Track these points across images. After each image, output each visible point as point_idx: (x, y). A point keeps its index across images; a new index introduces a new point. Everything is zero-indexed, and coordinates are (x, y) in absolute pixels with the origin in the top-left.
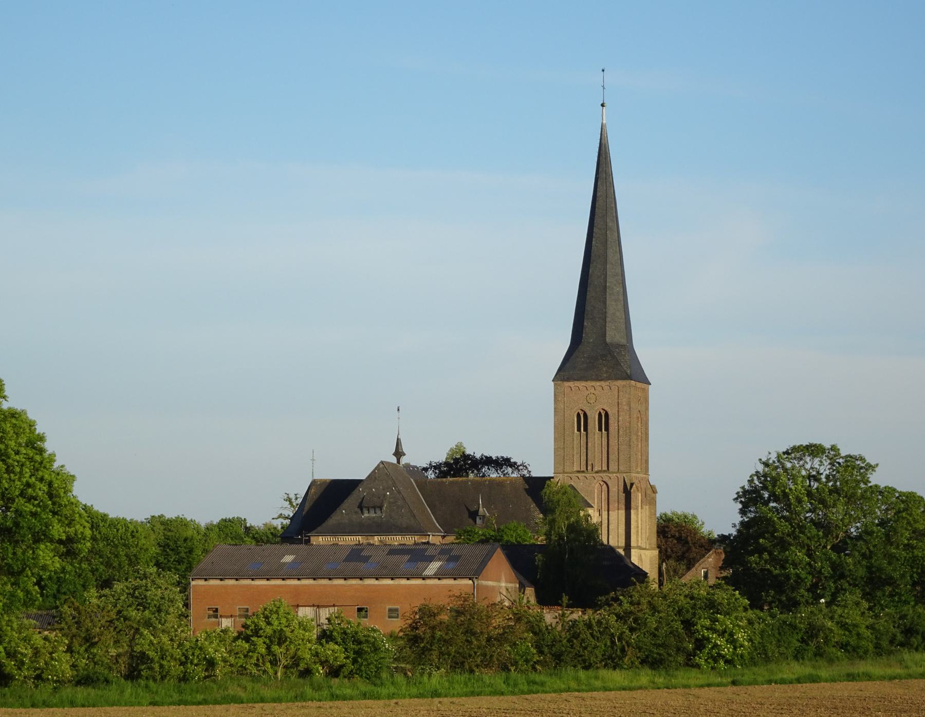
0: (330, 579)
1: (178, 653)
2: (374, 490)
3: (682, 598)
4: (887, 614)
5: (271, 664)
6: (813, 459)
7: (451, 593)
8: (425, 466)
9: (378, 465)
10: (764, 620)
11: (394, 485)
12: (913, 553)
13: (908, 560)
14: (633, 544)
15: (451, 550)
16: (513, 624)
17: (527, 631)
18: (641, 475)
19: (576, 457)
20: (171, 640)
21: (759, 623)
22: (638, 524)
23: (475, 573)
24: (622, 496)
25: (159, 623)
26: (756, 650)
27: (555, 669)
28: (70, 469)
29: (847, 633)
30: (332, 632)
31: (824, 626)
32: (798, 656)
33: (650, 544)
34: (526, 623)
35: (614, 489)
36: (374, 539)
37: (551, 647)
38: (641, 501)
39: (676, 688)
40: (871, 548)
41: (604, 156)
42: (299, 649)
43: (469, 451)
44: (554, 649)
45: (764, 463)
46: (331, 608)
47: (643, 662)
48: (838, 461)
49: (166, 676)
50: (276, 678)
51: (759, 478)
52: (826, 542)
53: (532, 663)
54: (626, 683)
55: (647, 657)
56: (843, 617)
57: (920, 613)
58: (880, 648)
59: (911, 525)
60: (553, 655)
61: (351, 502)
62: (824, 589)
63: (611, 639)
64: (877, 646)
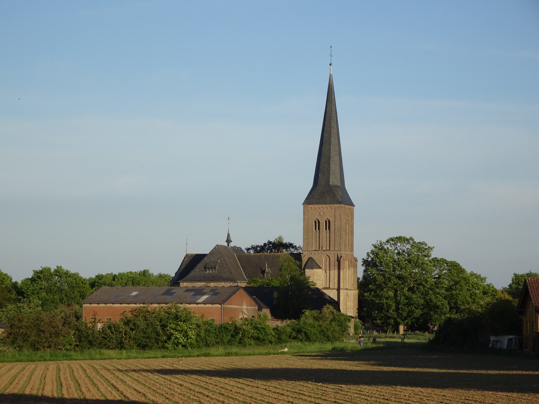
2: (212, 259)
8: (249, 247)
9: (215, 247)
14: (341, 287)
19: (314, 243)
24: (337, 263)
33: (353, 287)
58: (280, 340)
61: (200, 265)
64: (279, 339)
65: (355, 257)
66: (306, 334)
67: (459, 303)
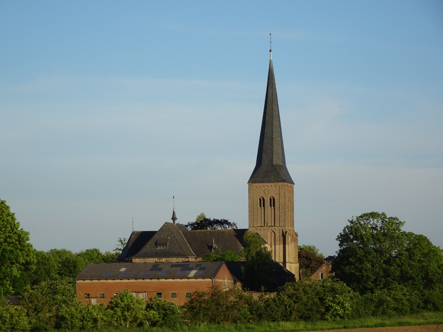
0: (143, 279)
1: (79, 316)
2: (162, 236)
3: (319, 287)
4: (416, 294)
5: (123, 321)
6: (374, 219)
7: (208, 286)
8: (186, 224)
9: (164, 224)
10: (358, 297)
11: (172, 233)
12: (422, 264)
13: (420, 268)
14: (287, 261)
15: (201, 265)
16: (238, 300)
17: (245, 304)
18: (290, 228)
19: (259, 220)
20: (76, 309)
21: (355, 299)
22: (289, 251)
23: (213, 276)
24: (282, 238)
25: (70, 301)
26: (354, 311)
27: (258, 322)
28: (25, 230)
29: (397, 303)
30: (152, 305)
31: (386, 300)
32: (374, 314)
33: (295, 261)
34: (245, 300)
35: (277, 235)
36: (163, 260)
37: (256, 311)
38: (291, 240)
39: (317, 330)
40: (402, 261)
41: (271, 75)
42: (137, 313)
43: (207, 217)
44: (258, 312)
45: (350, 222)
46: (144, 293)
47: (301, 318)
48: (385, 220)
49: (74, 327)
50: (126, 327)
51: (348, 229)
52: (381, 259)
53: (247, 319)
54: (293, 328)
55: (302, 315)
56: (395, 295)
57: (431, 293)
58: (412, 310)
59: (421, 251)
60: (257, 315)
61: (151, 242)
62: (380, 281)
63: (285, 307)
64: (411, 309)
66: (434, 304)
67: (430, 274)
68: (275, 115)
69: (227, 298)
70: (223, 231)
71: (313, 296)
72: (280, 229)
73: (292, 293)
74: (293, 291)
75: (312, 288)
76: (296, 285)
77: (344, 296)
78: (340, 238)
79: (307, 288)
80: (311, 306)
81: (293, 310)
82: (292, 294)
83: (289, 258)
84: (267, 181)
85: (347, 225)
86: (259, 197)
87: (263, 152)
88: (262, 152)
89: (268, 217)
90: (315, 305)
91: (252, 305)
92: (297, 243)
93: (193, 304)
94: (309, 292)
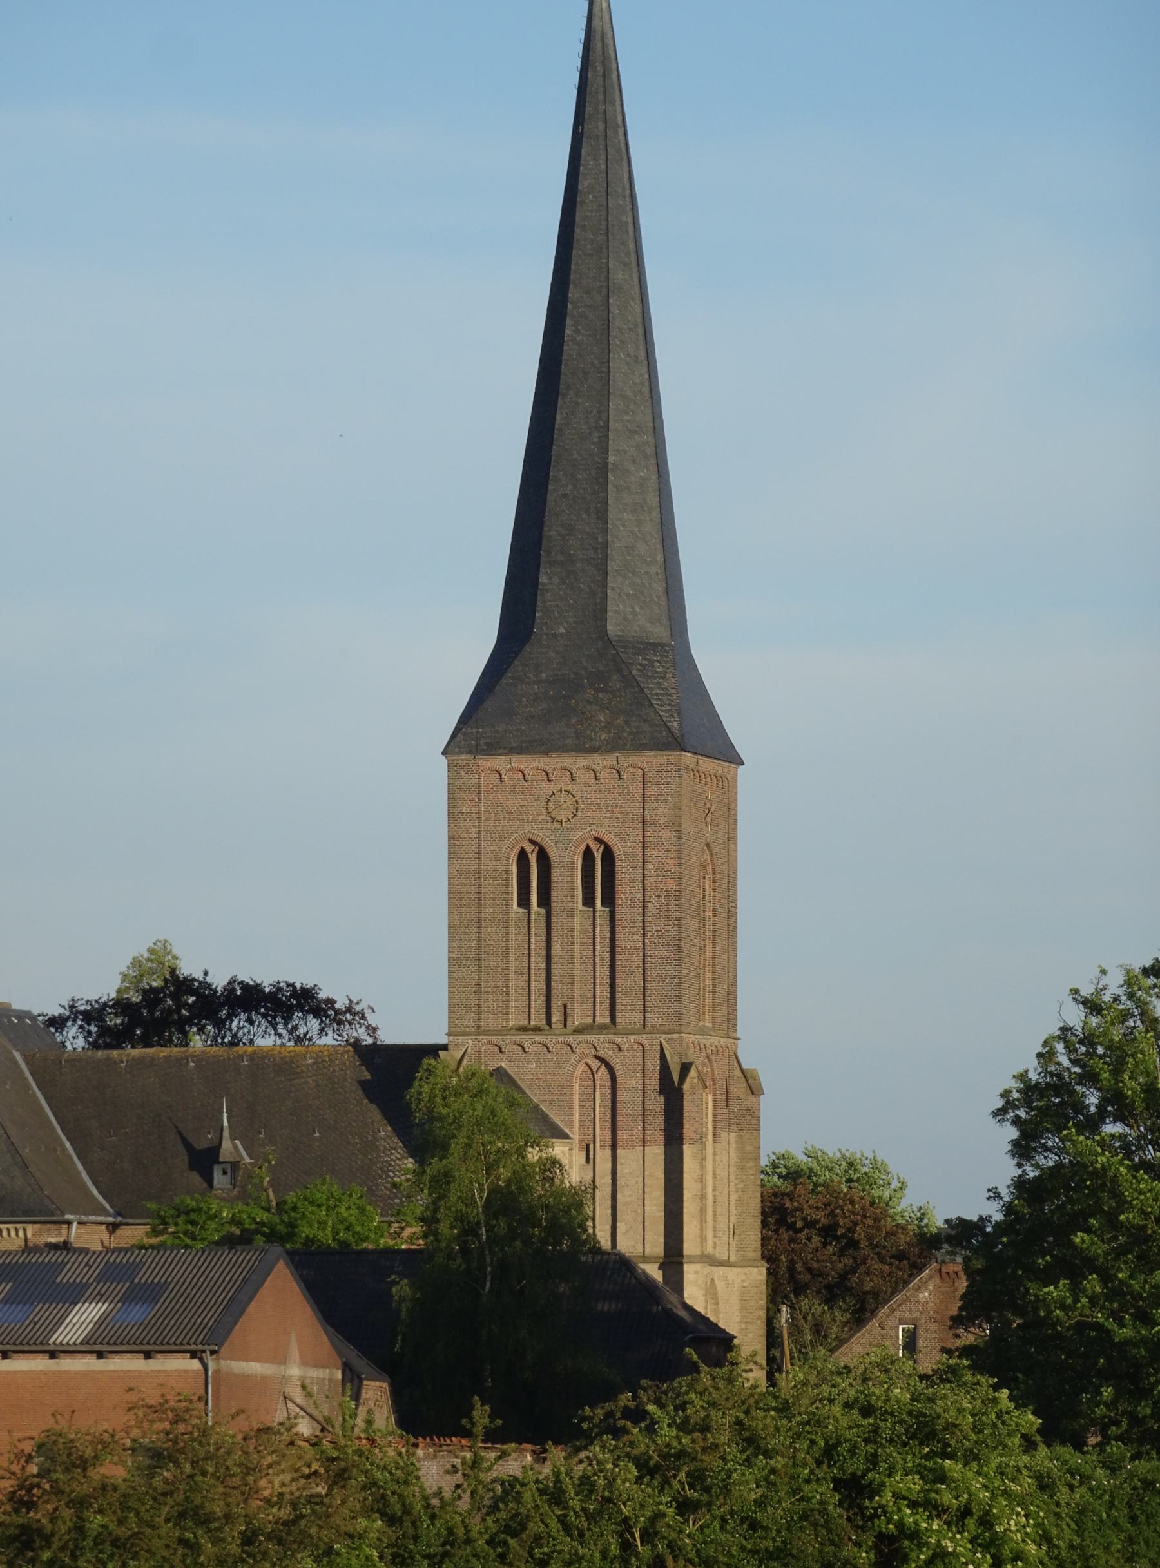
3: (837, 1409)
8: (56, 1011)
14: (690, 1247)
15: (137, 1266)
16: (321, 1490)
17: (368, 1512)
18: (713, 1040)
19: (516, 986)
21: (1071, 1487)
22: (703, 1188)
24: (657, 1103)
33: (739, 1249)
34: (364, 1488)
35: (630, 1083)
41: (600, 68)
43: (189, 968)
45: (1085, 1002)
51: (1070, 1048)
63: (621, 1536)
65: (744, 1067)
68: (618, 322)
69: (248, 1474)
70: (284, 1054)
71: (799, 1469)
72: (647, 1046)
73: (668, 1445)
74: (677, 1437)
75: (794, 1416)
76: (692, 1395)
77: (999, 1467)
78: (1018, 1108)
79: (763, 1421)
80: (789, 1529)
81: (675, 1558)
82: (665, 1456)
83: (701, 1229)
84: (569, 741)
85: (1062, 1025)
86: (516, 840)
87: (543, 559)
88: (540, 555)
89: (573, 968)
90: (815, 1525)
91: (413, 1523)
92: (758, 1138)
93: (31, 1514)
94: (772, 1443)
